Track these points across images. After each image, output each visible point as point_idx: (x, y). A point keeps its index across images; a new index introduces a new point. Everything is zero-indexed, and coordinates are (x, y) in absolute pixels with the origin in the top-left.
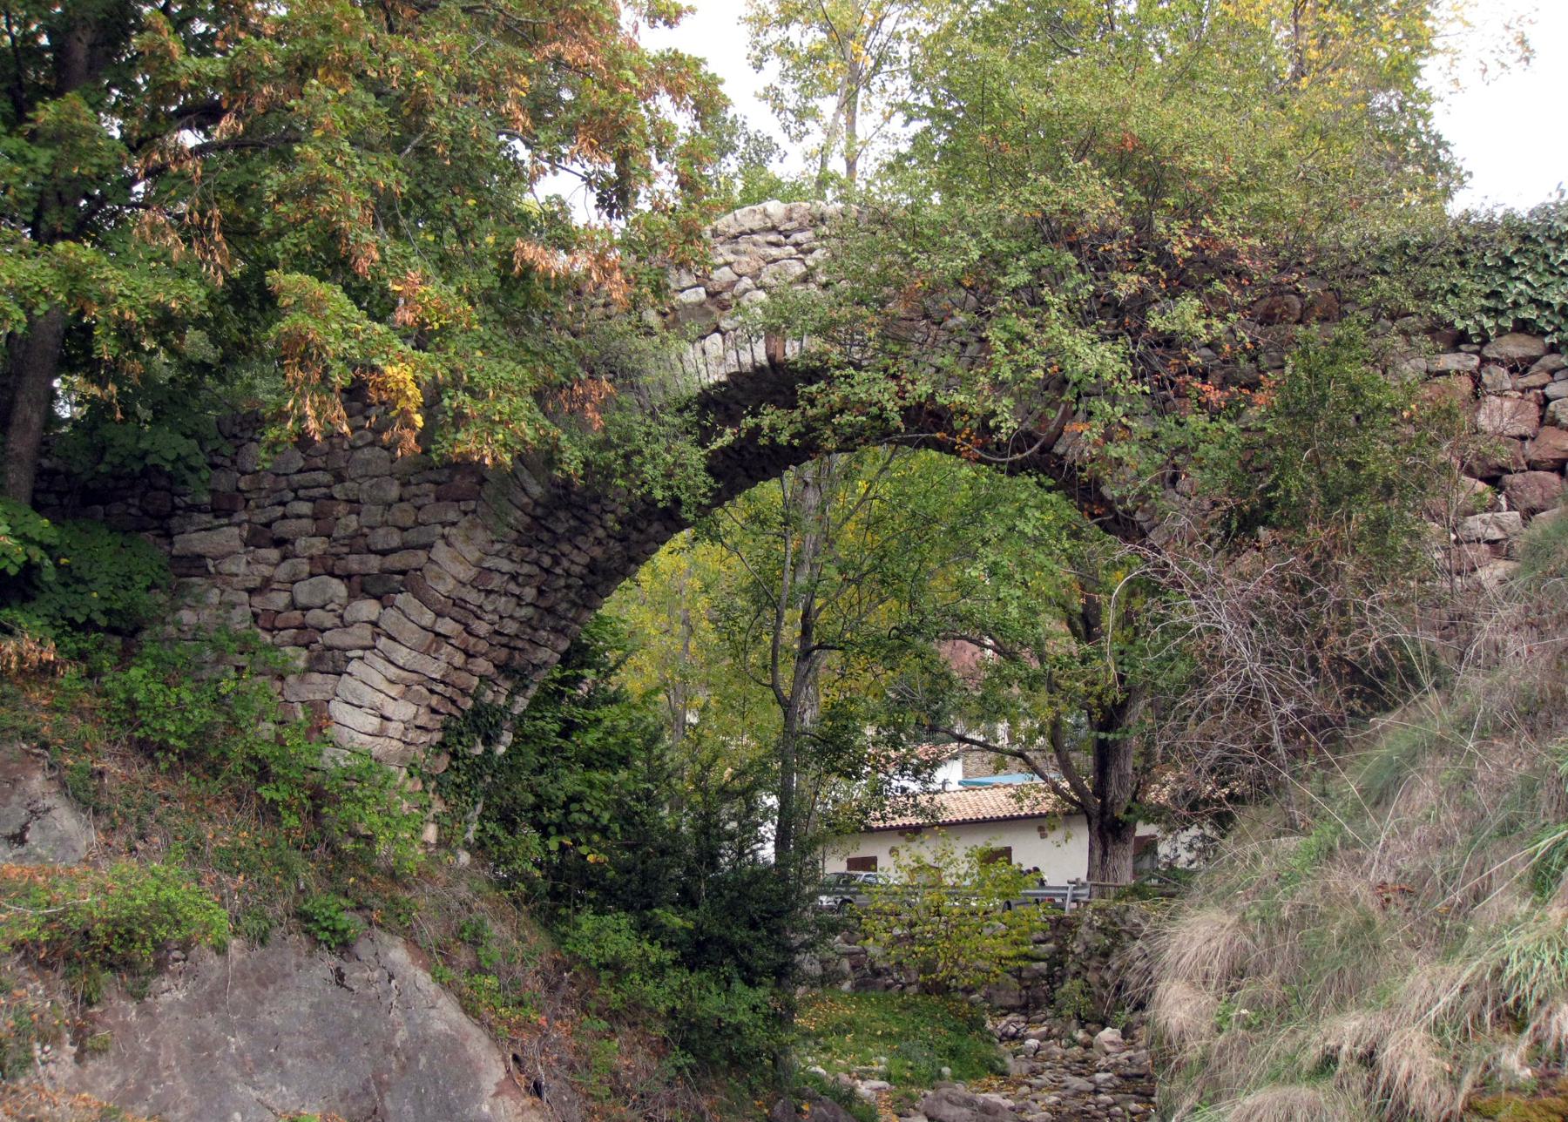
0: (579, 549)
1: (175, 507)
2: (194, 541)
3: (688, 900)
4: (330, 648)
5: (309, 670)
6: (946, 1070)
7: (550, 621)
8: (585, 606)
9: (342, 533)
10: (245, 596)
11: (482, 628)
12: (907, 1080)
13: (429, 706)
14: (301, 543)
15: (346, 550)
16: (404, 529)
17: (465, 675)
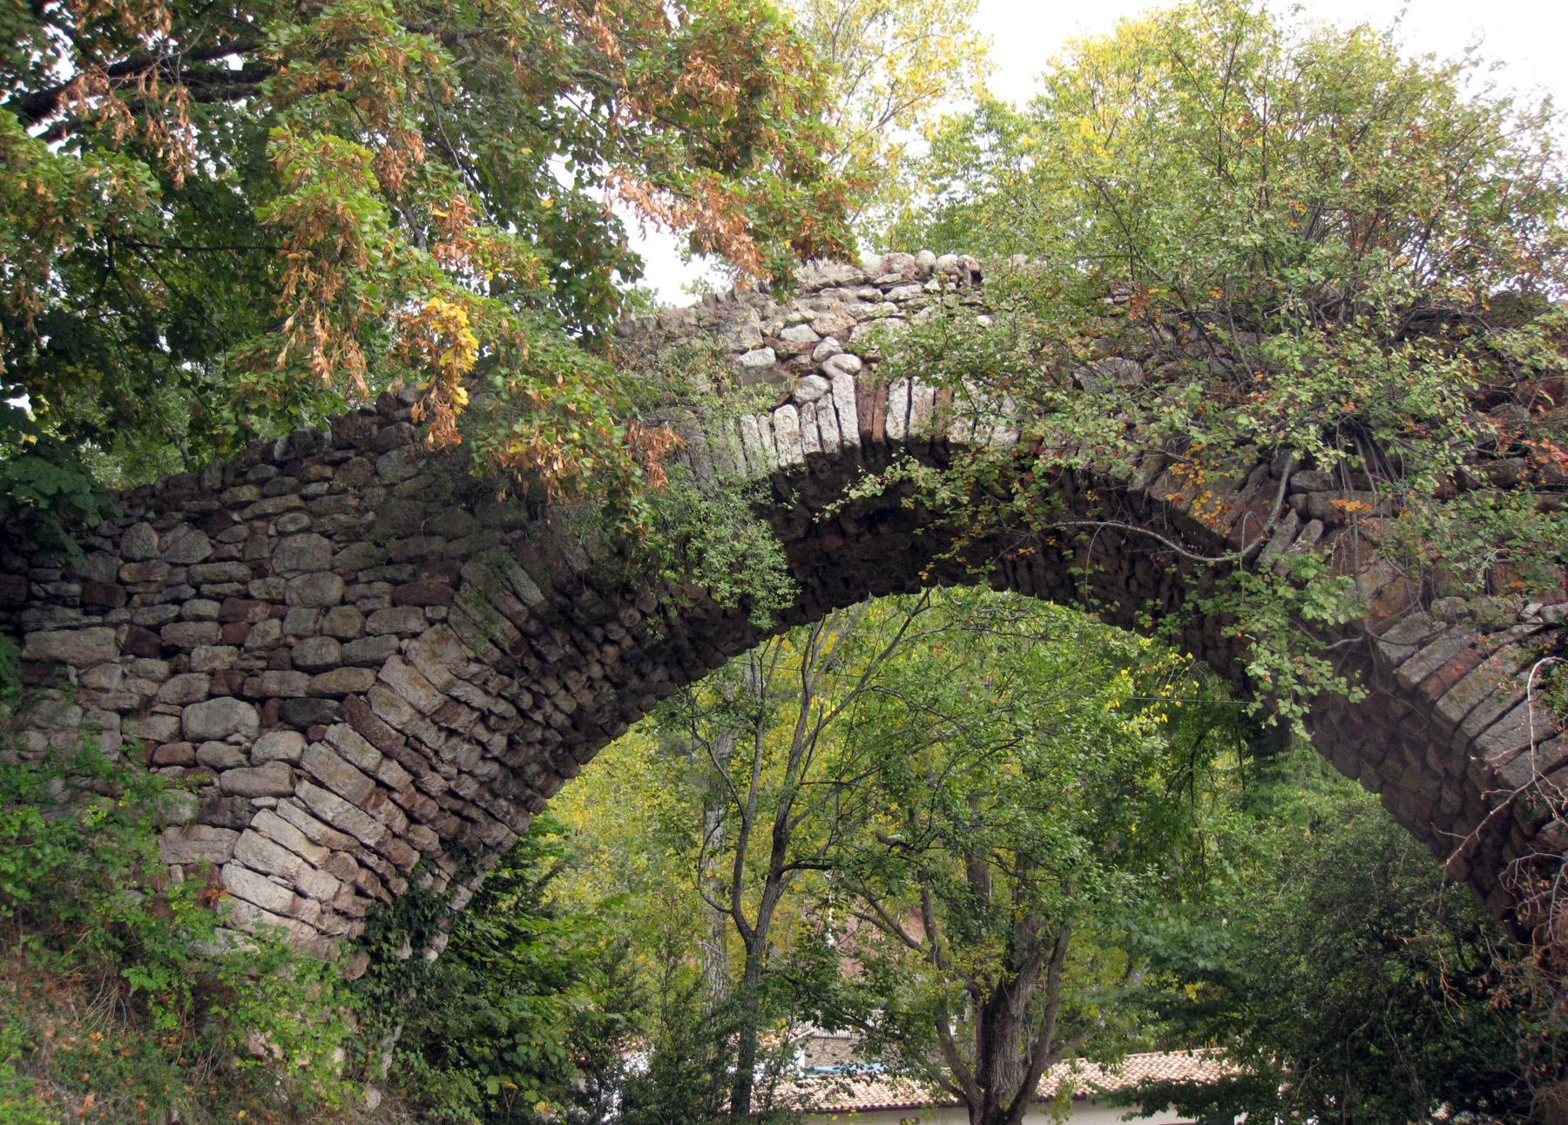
1: (32, 596)
2: (56, 642)
4: (230, 794)
5: (198, 821)
7: (514, 788)
8: (557, 772)
9: (259, 642)
11: (435, 783)
14: (200, 653)
15: (262, 664)
16: (343, 641)
17: (402, 844)
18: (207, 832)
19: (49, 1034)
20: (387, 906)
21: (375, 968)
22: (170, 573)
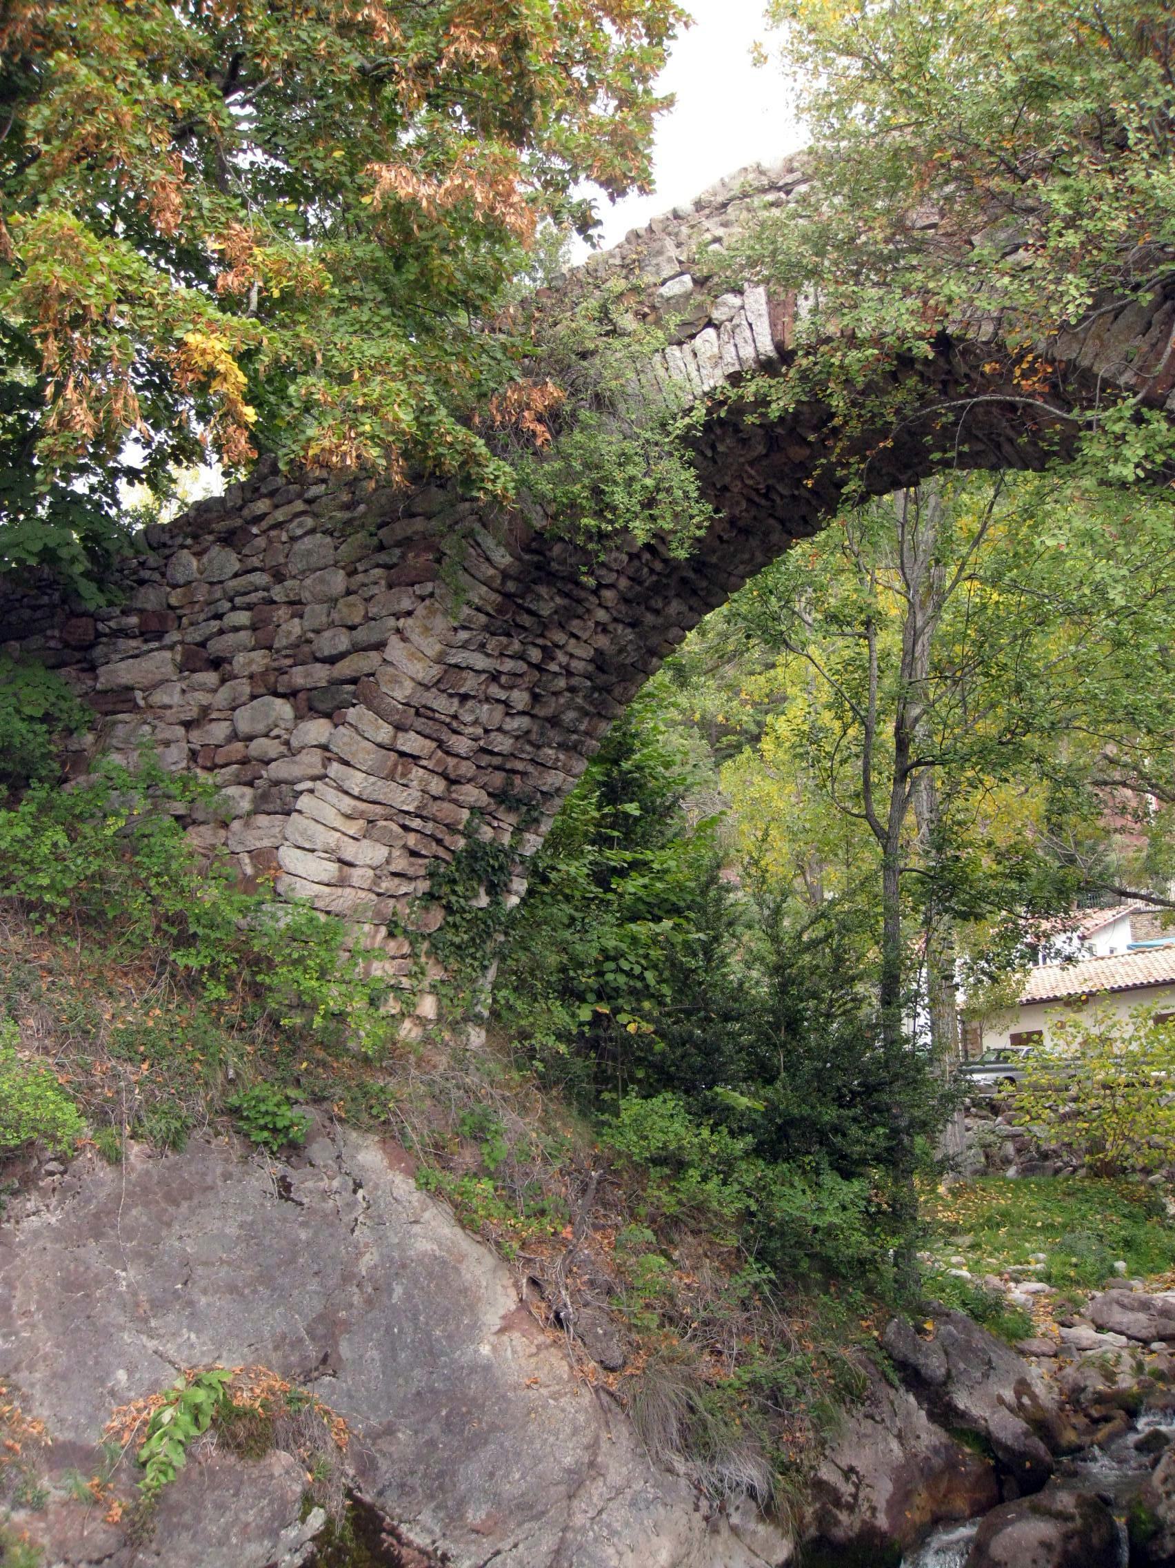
0: (577, 638)
1: (99, 634)
3: (763, 1074)
4: (277, 783)
5: (255, 812)
6: (1120, 1265)
7: (555, 736)
8: (599, 715)
9: (284, 642)
10: (180, 731)
11: (462, 745)
12: (1070, 1279)
13: (405, 847)
14: (240, 659)
15: (289, 662)
16: (352, 628)
17: (446, 805)
18: (262, 820)
19: (107, 1016)
20: (448, 863)
21: (450, 919)
22: (210, 593)
